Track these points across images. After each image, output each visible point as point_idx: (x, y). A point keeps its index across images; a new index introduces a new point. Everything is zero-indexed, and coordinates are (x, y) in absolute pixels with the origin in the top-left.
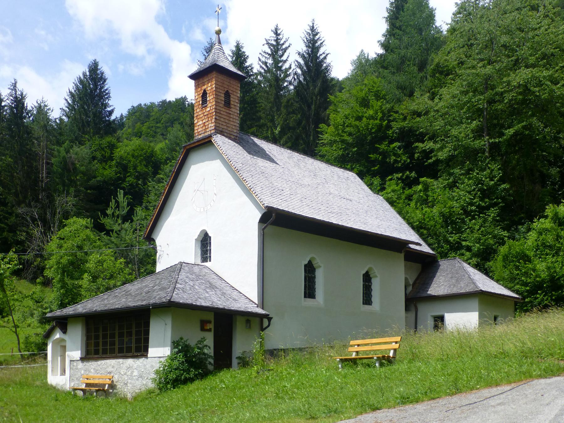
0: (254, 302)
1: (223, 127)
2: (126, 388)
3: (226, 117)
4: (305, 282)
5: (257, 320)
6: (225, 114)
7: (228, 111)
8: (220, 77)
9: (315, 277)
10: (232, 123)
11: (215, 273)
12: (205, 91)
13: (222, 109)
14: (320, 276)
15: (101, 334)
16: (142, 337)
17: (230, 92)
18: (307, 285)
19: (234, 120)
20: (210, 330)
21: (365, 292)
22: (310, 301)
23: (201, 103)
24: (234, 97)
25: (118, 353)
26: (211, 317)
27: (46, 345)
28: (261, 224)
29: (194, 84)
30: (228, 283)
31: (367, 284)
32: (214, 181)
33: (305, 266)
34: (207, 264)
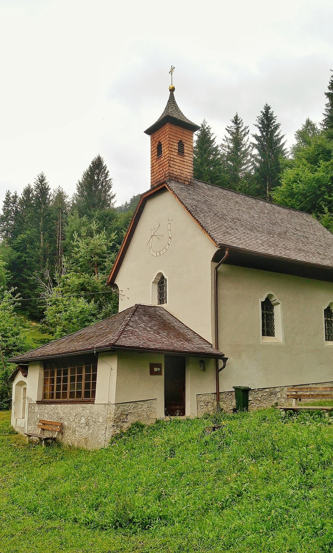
0: (208, 342)
1: (176, 174)
2: (74, 435)
3: (180, 165)
4: (263, 320)
5: (213, 361)
6: (178, 161)
7: (182, 159)
8: (173, 128)
9: (273, 314)
10: (186, 170)
11: (170, 314)
12: (160, 142)
13: (175, 157)
14: (278, 312)
15: (84, 374)
16: (91, 382)
17: (184, 141)
18: (265, 323)
19: (188, 168)
20: (159, 373)
21: (327, 327)
22: (268, 339)
23: (156, 154)
24: (188, 146)
25: (70, 398)
26: (161, 360)
27: (10, 389)
28: (213, 263)
29: (149, 142)
30: (183, 324)
31: (329, 319)
32: (169, 225)
33: (263, 303)
34: (164, 306)
